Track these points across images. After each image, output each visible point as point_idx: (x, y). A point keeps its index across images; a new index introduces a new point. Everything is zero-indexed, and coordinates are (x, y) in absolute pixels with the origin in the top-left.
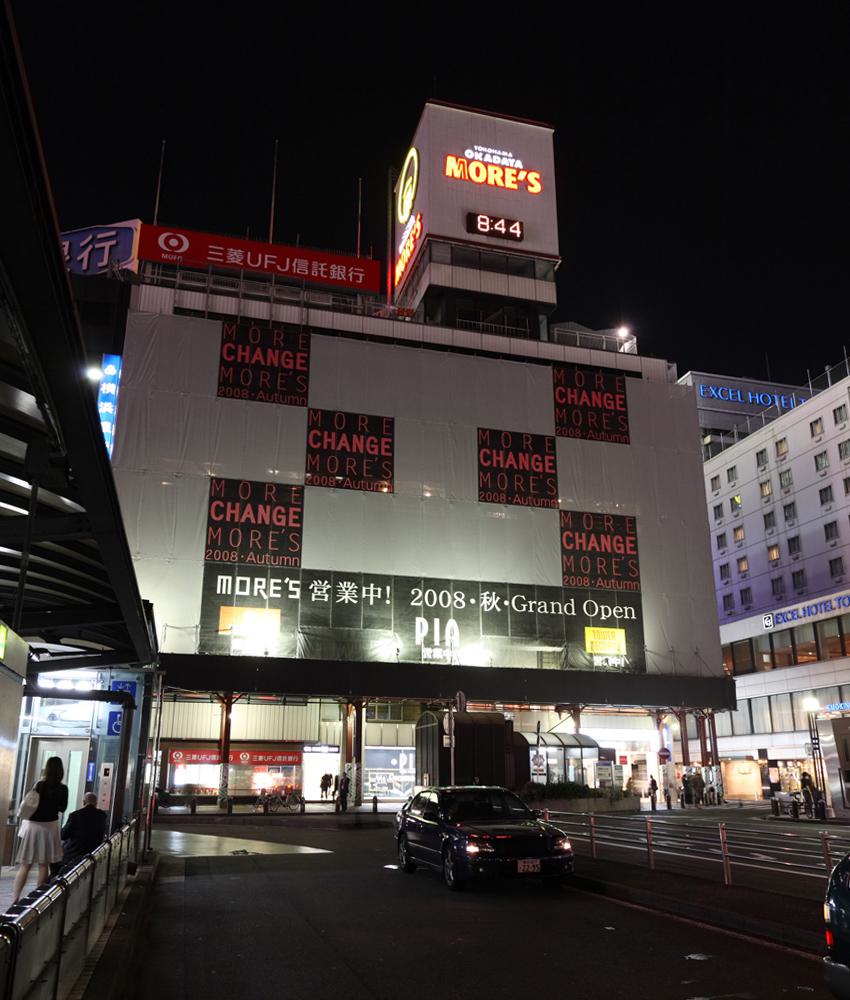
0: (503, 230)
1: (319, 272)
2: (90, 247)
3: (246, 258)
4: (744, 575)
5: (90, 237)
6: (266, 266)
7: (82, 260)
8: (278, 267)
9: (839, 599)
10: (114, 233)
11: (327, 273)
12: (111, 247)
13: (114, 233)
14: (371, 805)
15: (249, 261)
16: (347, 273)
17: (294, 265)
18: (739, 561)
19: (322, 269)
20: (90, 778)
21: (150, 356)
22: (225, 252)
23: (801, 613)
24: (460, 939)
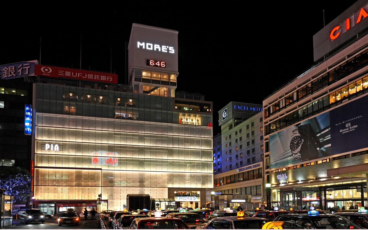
0: (159, 65)
1: (97, 78)
2: (22, 68)
3: (72, 74)
4: (241, 158)
5: (21, 65)
6: (79, 77)
7: (19, 72)
8: (83, 77)
9: (253, 166)
10: (29, 64)
11: (100, 78)
12: (28, 68)
13: (29, 64)
15: (73, 75)
16: (106, 78)
17: (88, 76)
18: (241, 154)
19: (98, 77)
22: (64, 73)
23: (252, 167)
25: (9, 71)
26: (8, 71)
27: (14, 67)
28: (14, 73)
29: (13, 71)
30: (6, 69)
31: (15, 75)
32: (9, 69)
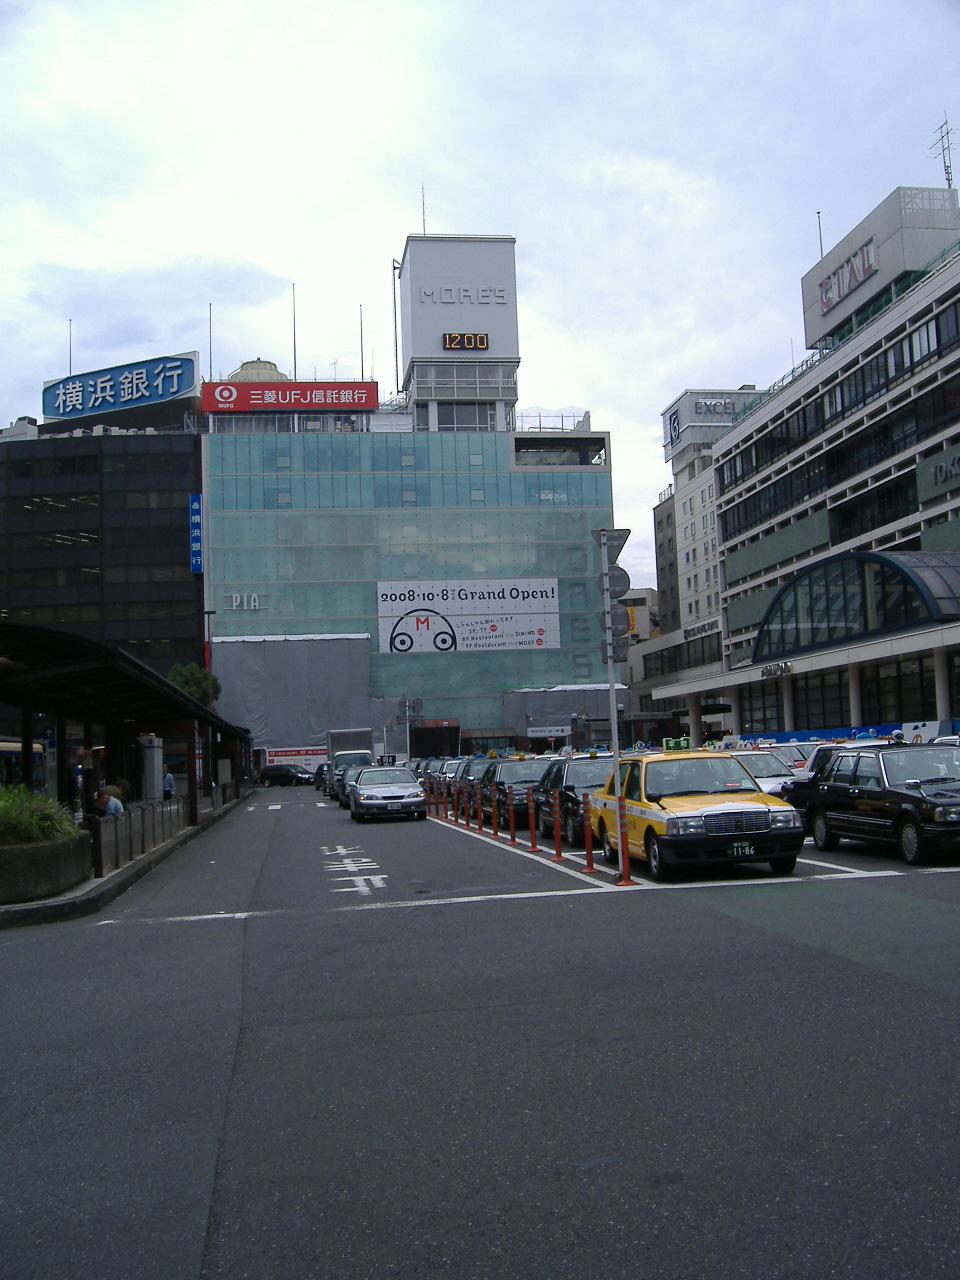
2: (163, 375)
5: (161, 366)
10: (178, 363)
14: (767, 704)
16: (354, 395)
20: (745, 663)
21: (211, 557)
22: (263, 395)
24: (875, 1147)
25: (135, 382)
26: (131, 382)
27: (144, 371)
28: (145, 388)
29: (143, 383)
30: (126, 378)
31: (147, 394)
32: (135, 377)
